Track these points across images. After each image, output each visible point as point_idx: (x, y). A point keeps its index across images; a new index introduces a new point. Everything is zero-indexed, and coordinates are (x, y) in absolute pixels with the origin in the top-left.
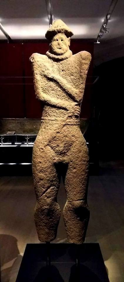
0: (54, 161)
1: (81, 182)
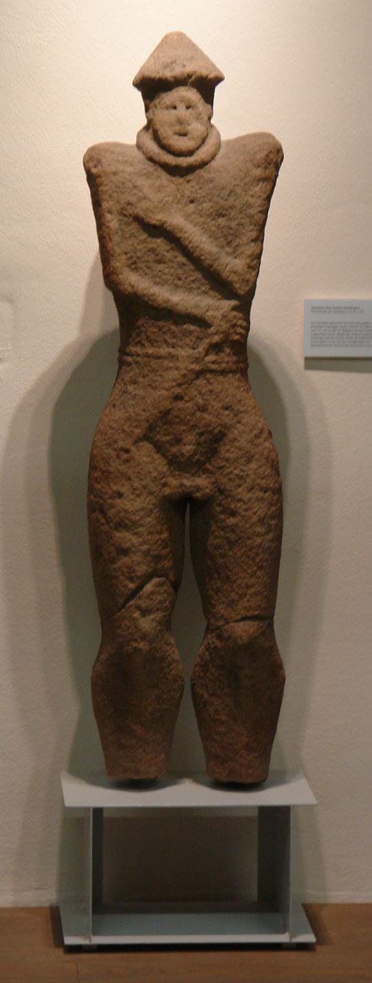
0: (165, 489)
1: (253, 559)
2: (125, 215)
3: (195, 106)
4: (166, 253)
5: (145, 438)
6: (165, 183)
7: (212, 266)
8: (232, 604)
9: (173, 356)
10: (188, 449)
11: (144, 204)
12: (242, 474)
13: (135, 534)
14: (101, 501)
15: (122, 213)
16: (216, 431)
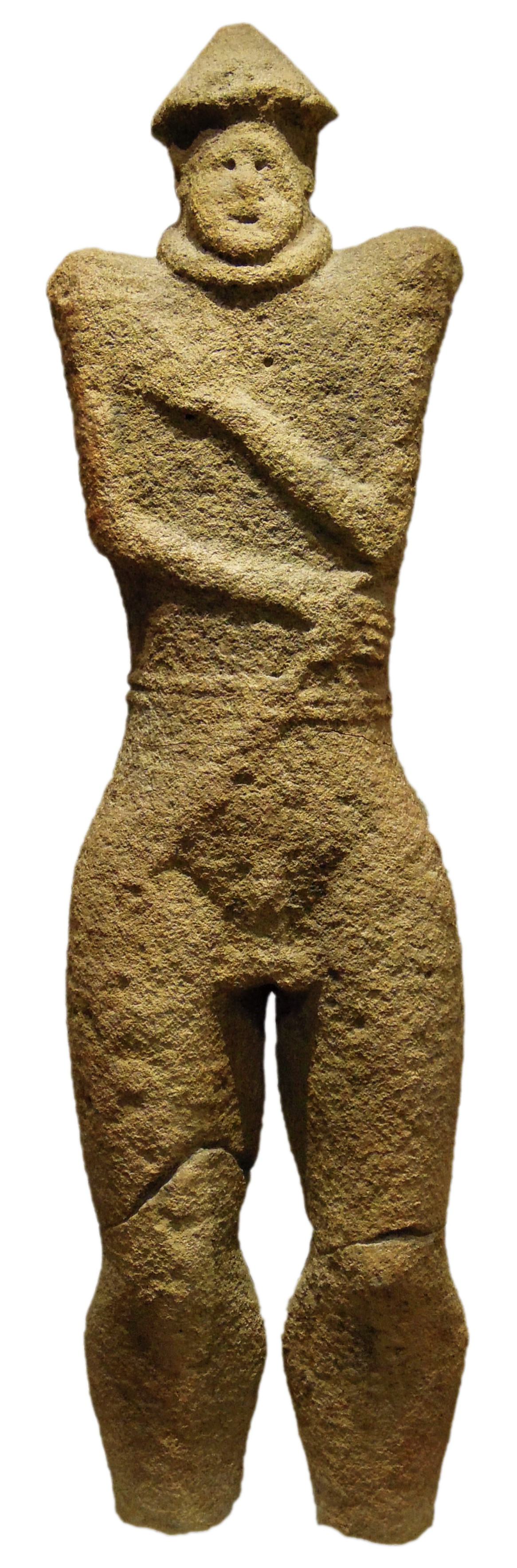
0: (218, 969)
1: (402, 1115)
2: (128, 393)
3: (275, 162)
4: (214, 472)
5: (176, 863)
6: (213, 322)
7: (310, 497)
8: (359, 1204)
9: (231, 690)
10: (263, 886)
11: (166, 368)
12: (379, 937)
13: (154, 1062)
14: (87, 994)
15: (121, 387)
16: (323, 847)
